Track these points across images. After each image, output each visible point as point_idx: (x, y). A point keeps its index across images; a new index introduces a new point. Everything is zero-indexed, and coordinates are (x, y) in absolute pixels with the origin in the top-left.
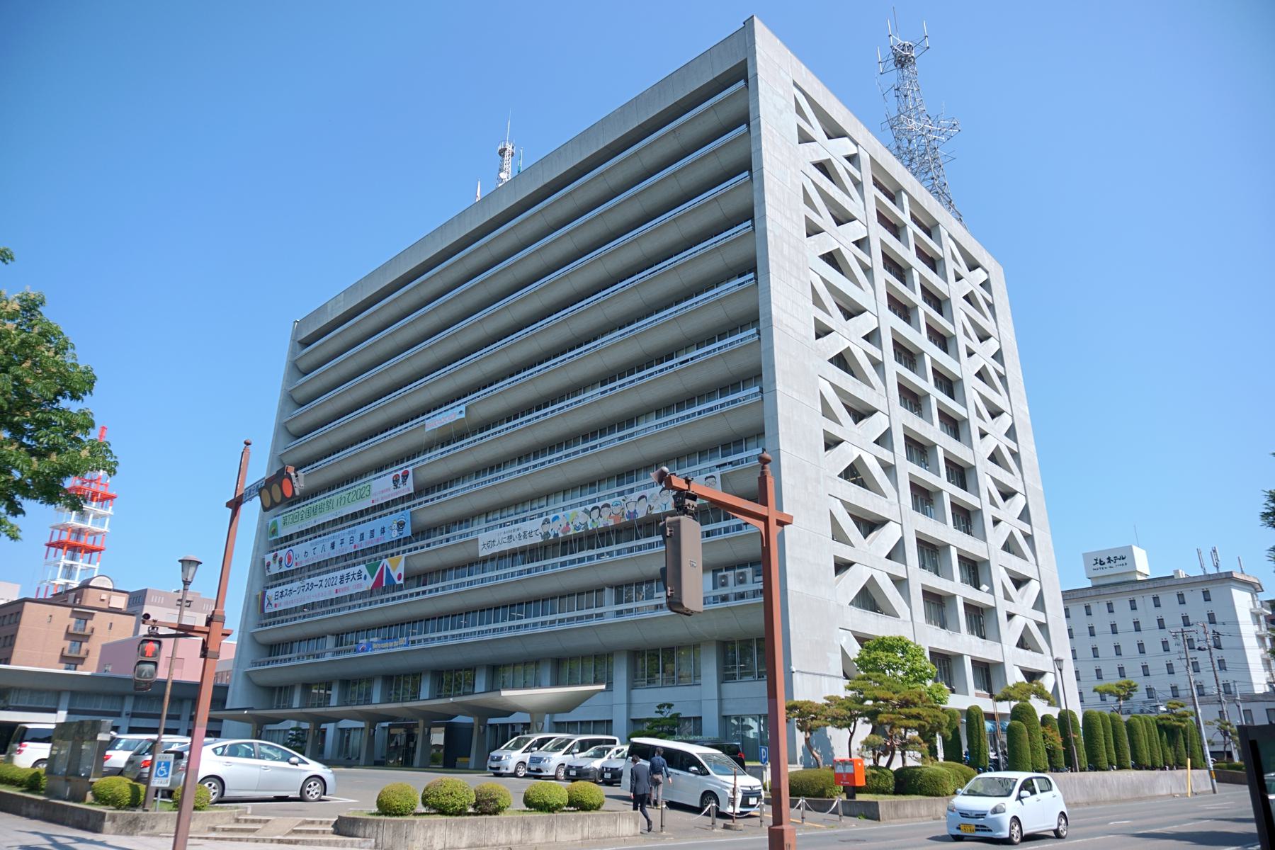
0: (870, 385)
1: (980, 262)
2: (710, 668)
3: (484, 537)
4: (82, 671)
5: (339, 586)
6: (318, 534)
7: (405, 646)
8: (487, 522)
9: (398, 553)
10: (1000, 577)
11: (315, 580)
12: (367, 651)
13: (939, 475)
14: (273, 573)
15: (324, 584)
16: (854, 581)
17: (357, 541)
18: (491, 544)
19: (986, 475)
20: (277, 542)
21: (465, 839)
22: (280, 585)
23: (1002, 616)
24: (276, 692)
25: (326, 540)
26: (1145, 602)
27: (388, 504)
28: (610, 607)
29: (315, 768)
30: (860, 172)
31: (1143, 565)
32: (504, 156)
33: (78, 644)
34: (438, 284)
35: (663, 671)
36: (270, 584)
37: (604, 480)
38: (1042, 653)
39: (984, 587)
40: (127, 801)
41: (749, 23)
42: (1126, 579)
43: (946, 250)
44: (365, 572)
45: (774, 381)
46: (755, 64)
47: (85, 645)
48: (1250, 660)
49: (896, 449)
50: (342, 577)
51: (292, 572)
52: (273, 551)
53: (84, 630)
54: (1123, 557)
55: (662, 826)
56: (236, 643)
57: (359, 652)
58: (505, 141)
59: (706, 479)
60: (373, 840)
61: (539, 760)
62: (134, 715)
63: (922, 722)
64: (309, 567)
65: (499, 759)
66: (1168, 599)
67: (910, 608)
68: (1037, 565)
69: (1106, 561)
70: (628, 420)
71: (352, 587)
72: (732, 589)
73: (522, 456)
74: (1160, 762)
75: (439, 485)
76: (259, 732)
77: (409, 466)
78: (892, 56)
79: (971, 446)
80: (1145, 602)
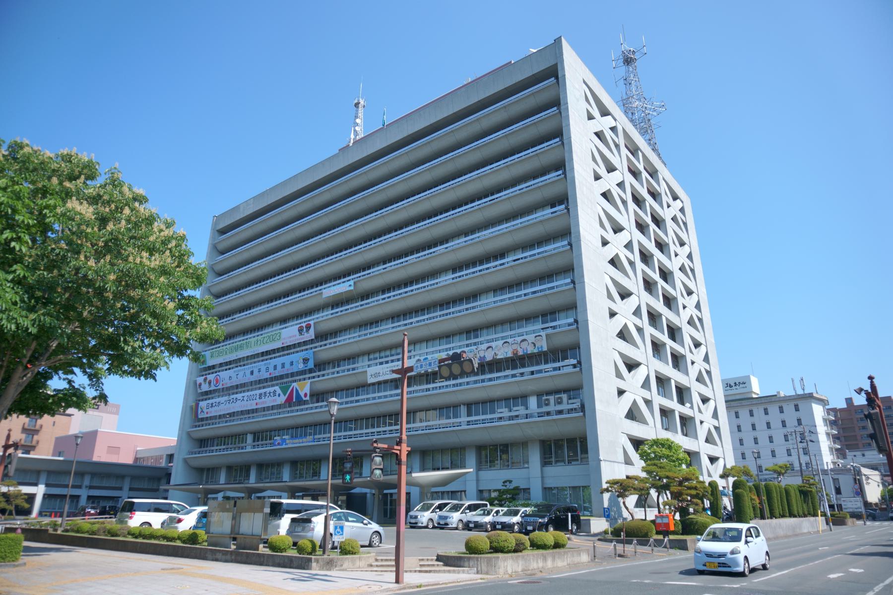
0: (629, 277)
1: (679, 195)
2: (535, 457)
3: (371, 371)
4: (34, 455)
5: (258, 401)
6: (239, 364)
7: (312, 442)
8: (369, 360)
9: (304, 379)
10: (696, 399)
11: (239, 396)
12: (282, 445)
13: (664, 334)
14: (203, 390)
15: (245, 399)
16: (625, 403)
17: (271, 370)
18: (377, 375)
19: (687, 331)
20: (206, 369)
21: (520, 566)
22: (209, 399)
23: (698, 423)
24: (205, 472)
25: (247, 369)
26: (759, 412)
27: (294, 346)
28: (464, 419)
29: (375, 527)
30: (618, 138)
31: (757, 388)
32: (358, 107)
33: (31, 436)
34: (327, 197)
35: (501, 459)
36: (201, 398)
37: (384, 320)
38: (717, 445)
39: (688, 405)
40: (310, 550)
41: (558, 42)
42: (746, 397)
43: (662, 189)
44: (279, 391)
45: (583, 276)
46: (563, 69)
47: (36, 437)
48: (822, 449)
49: (643, 319)
50: (260, 395)
51: (215, 391)
52: (203, 376)
53: (35, 426)
54: (744, 382)
55: (595, 556)
56: (176, 439)
57: (275, 445)
58: (359, 97)
59: (536, 337)
60: (476, 569)
61: (446, 518)
62: (91, 487)
63: (698, 492)
64: (232, 387)
65: (416, 517)
66: (773, 409)
67: (654, 419)
68: (713, 390)
69: (733, 385)
70: (473, 296)
71: (269, 402)
72: (552, 408)
73: (394, 317)
74: (801, 513)
75: (331, 334)
76: (206, 499)
77: (312, 320)
78: (621, 57)
79: (678, 314)
80: (759, 412)
